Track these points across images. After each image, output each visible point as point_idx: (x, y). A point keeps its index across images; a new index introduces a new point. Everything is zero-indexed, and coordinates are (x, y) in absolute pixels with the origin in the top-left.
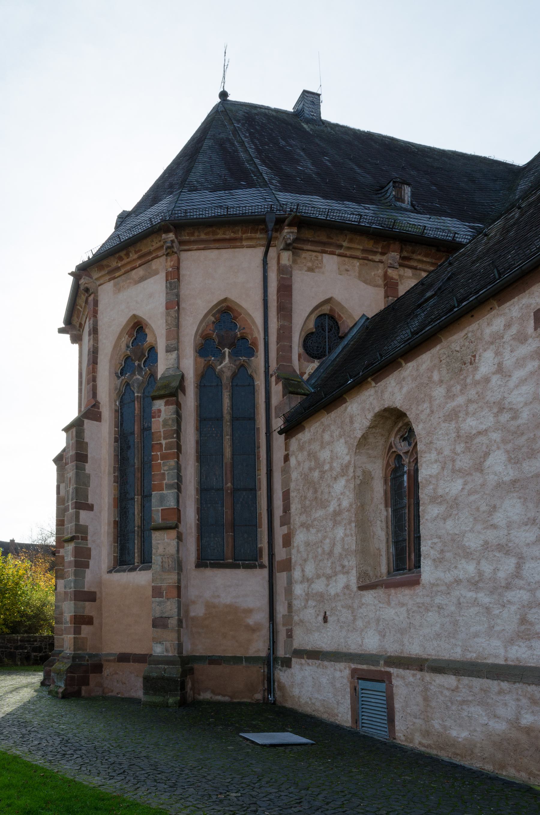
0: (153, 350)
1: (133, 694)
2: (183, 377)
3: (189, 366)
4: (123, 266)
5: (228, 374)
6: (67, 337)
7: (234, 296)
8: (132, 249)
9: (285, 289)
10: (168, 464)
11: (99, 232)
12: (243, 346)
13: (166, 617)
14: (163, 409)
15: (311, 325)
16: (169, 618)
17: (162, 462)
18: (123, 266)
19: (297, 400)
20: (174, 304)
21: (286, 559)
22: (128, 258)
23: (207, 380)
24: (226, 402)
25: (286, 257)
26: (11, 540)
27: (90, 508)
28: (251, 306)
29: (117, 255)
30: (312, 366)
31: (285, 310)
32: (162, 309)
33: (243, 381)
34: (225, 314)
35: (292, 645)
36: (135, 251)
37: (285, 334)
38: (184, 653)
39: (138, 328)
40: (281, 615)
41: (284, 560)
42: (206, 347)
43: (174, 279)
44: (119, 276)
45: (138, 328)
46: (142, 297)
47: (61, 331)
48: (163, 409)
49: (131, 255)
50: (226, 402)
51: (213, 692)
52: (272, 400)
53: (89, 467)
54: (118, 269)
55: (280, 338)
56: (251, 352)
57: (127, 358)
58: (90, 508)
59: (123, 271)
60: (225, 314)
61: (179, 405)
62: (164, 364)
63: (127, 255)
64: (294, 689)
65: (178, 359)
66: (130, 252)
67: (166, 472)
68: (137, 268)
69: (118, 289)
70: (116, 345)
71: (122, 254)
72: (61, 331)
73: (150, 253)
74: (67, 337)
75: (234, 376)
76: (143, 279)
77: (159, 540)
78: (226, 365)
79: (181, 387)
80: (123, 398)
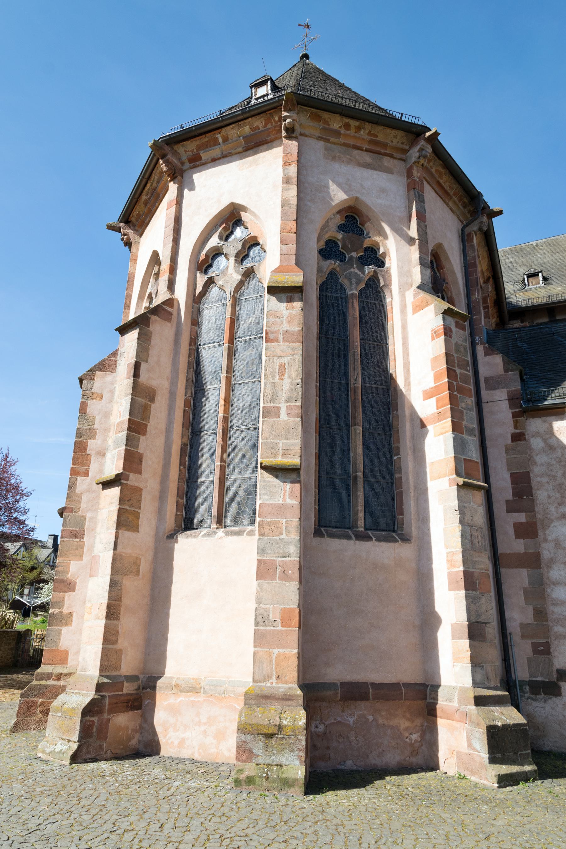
1: (373, 762)
4: (346, 135)
8: (368, 126)
10: (465, 401)
13: (482, 623)
16: (486, 623)
17: (459, 395)
18: (346, 135)
21: (525, 553)
22: (356, 132)
29: (347, 120)
35: (550, 663)
36: (370, 132)
38: (123, 667)
41: (520, 554)
44: (334, 143)
49: (362, 132)
54: (337, 134)
59: (342, 140)
63: (358, 129)
66: (364, 128)
67: (465, 411)
68: (362, 150)
71: (354, 123)
73: (385, 146)
77: (465, 502)
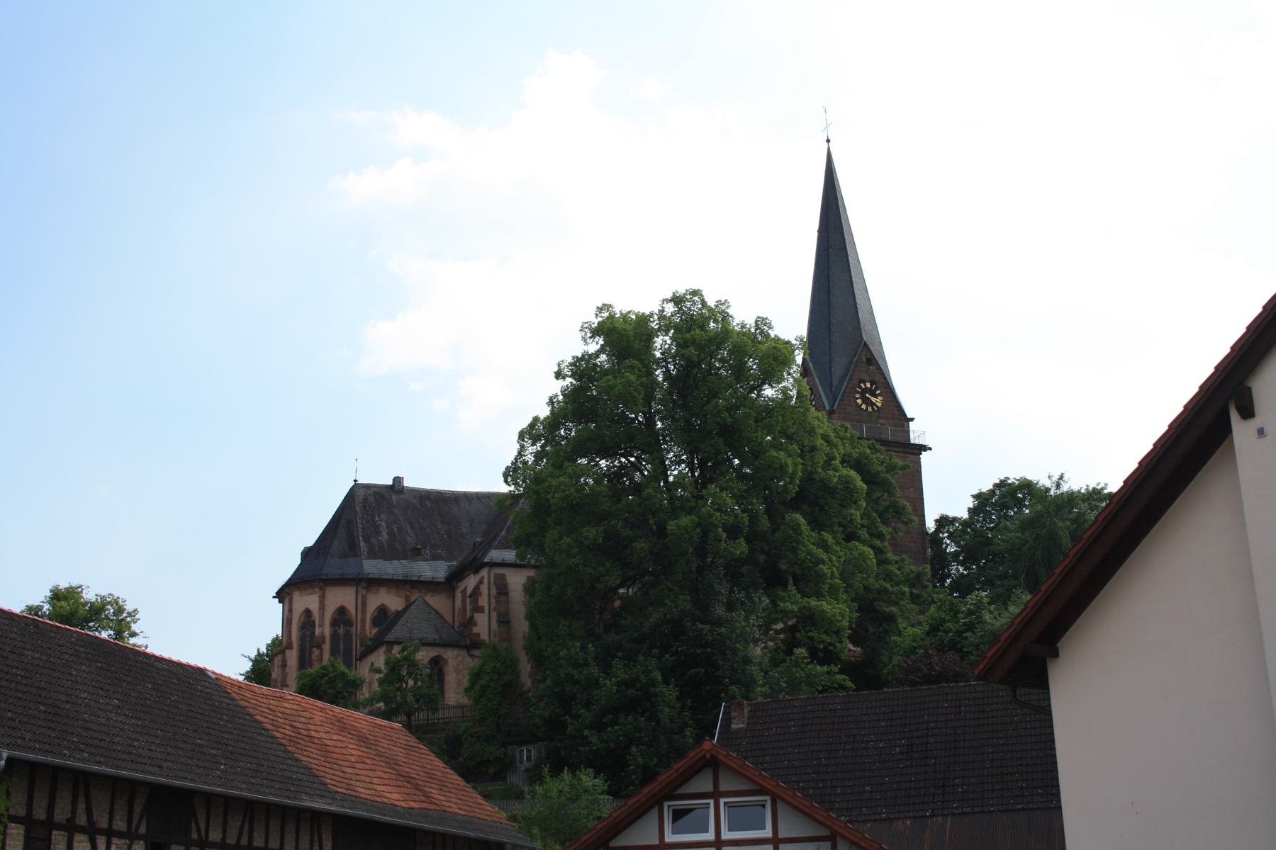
3: (327, 632)
7: (346, 605)
9: (364, 603)
11: (289, 564)
12: (349, 623)
14: (316, 651)
20: (322, 608)
23: (334, 636)
25: (364, 592)
26: (30, 609)
30: (375, 631)
31: (364, 612)
34: (342, 611)
37: (363, 621)
39: (308, 612)
42: (335, 623)
45: (308, 612)
46: (307, 601)
48: (316, 651)
51: (767, 511)
52: (357, 648)
56: (351, 625)
60: (342, 611)
62: (318, 631)
64: (855, 615)
65: (324, 629)
78: (341, 631)
79: (324, 642)
80: (302, 639)
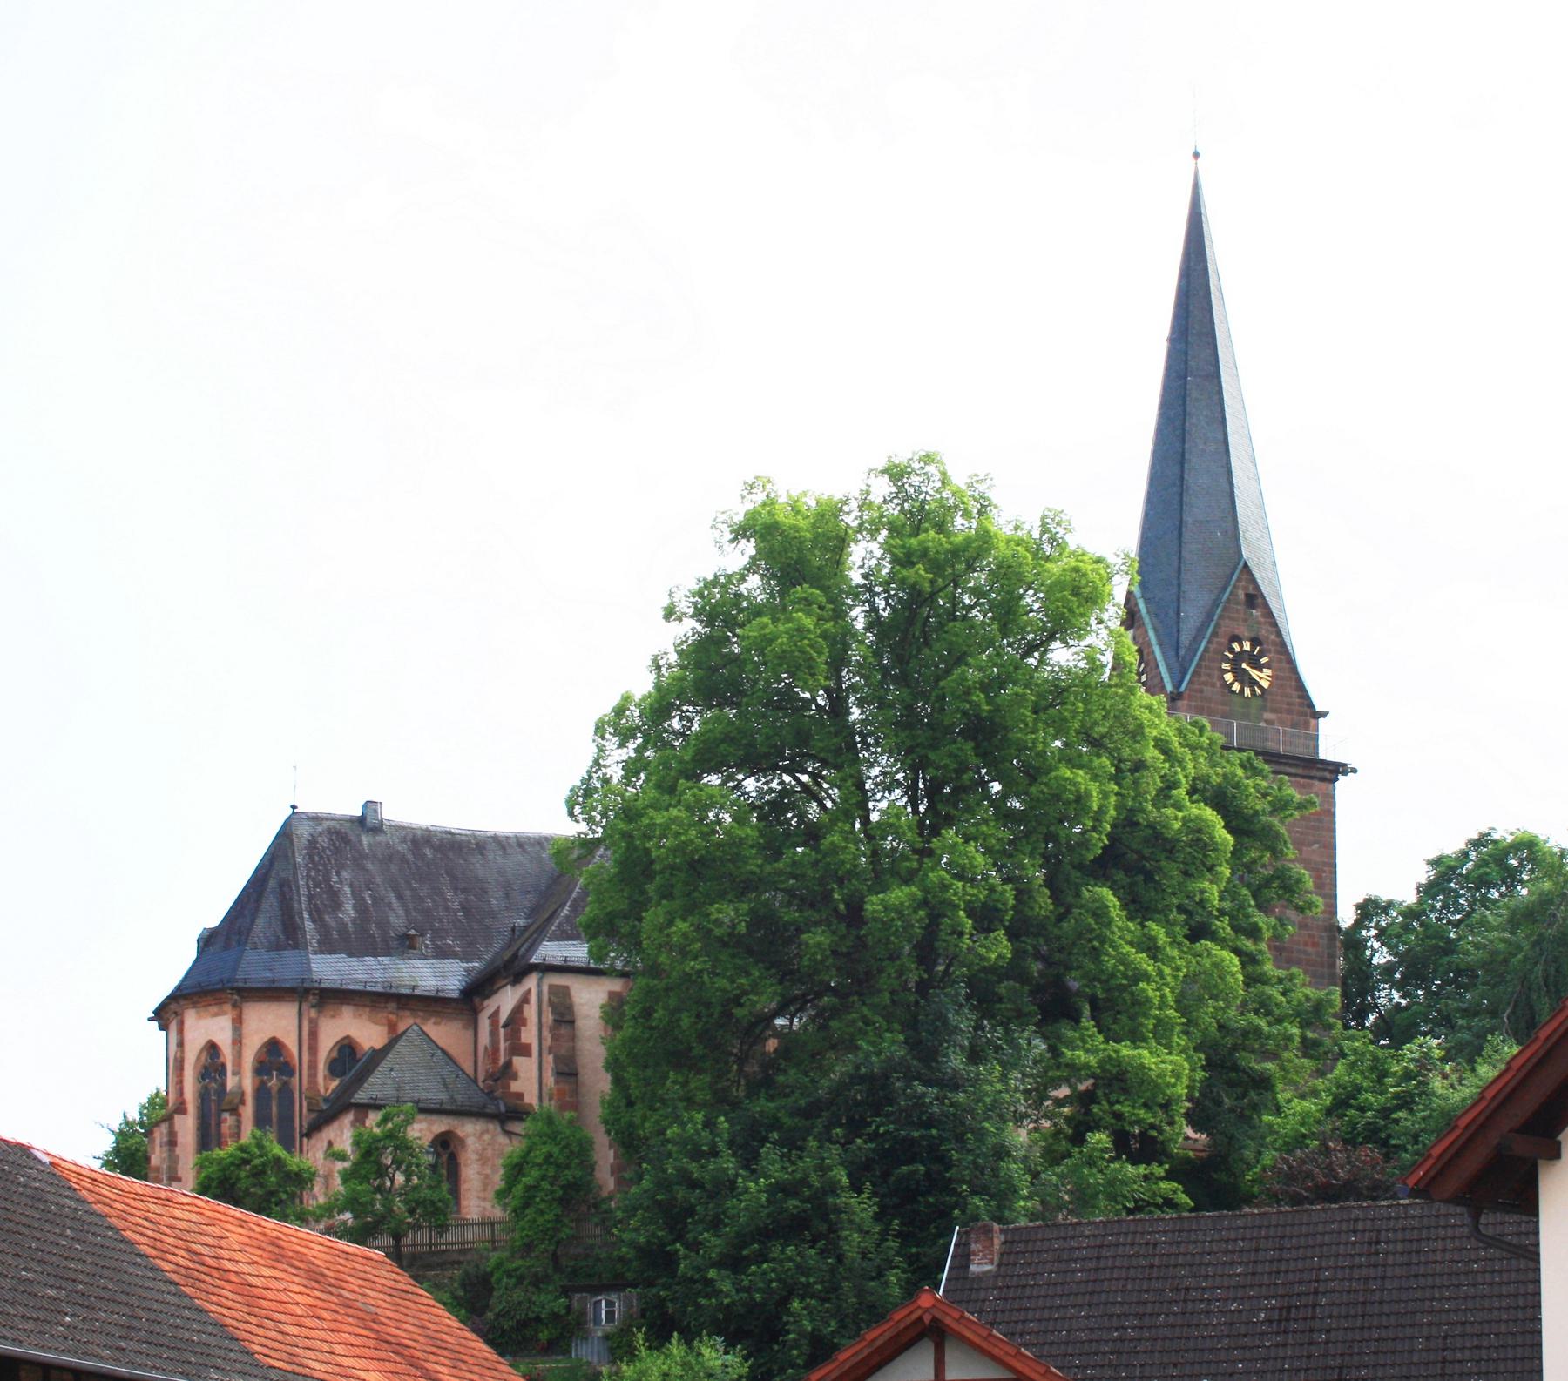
0: (223, 1066)
2: (243, 1094)
3: (248, 1084)
5: (275, 1090)
6: (155, 1024)
7: (279, 1036)
9: (314, 1035)
12: (286, 1069)
15: (335, 1054)
19: (314, 1115)
20: (238, 1041)
23: (261, 1092)
24: (274, 1109)
25: (313, 1013)
27: (179, 1180)
28: (291, 1042)
30: (334, 1084)
31: (313, 1050)
32: (229, 1041)
33: (285, 1092)
37: (313, 1066)
39: (212, 1048)
40: (598, 1098)
42: (261, 1068)
43: (238, 1023)
47: (150, 1019)
50: (274, 1109)
53: (178, 1150)
55: (309, 1076)
56: (291, 1074)
57: (205, 1068)
58: (179, 1180)
61: (239, 1115)
62: (231, 1082)
69: (199, 1017)
70: (198, 1058)
72: (150, 1019)
74: (155, 1024)
75: (280, 1091)
76: (216, 1015)
78: (274, 1083)
79: (243, 1102)
